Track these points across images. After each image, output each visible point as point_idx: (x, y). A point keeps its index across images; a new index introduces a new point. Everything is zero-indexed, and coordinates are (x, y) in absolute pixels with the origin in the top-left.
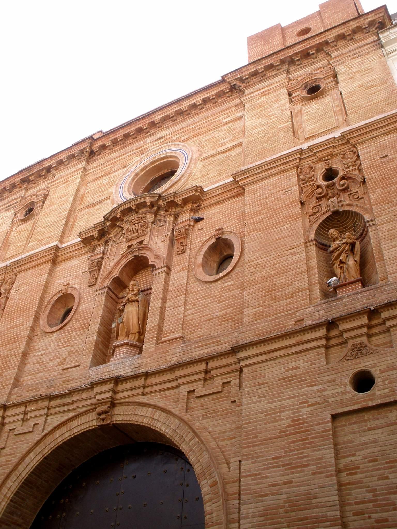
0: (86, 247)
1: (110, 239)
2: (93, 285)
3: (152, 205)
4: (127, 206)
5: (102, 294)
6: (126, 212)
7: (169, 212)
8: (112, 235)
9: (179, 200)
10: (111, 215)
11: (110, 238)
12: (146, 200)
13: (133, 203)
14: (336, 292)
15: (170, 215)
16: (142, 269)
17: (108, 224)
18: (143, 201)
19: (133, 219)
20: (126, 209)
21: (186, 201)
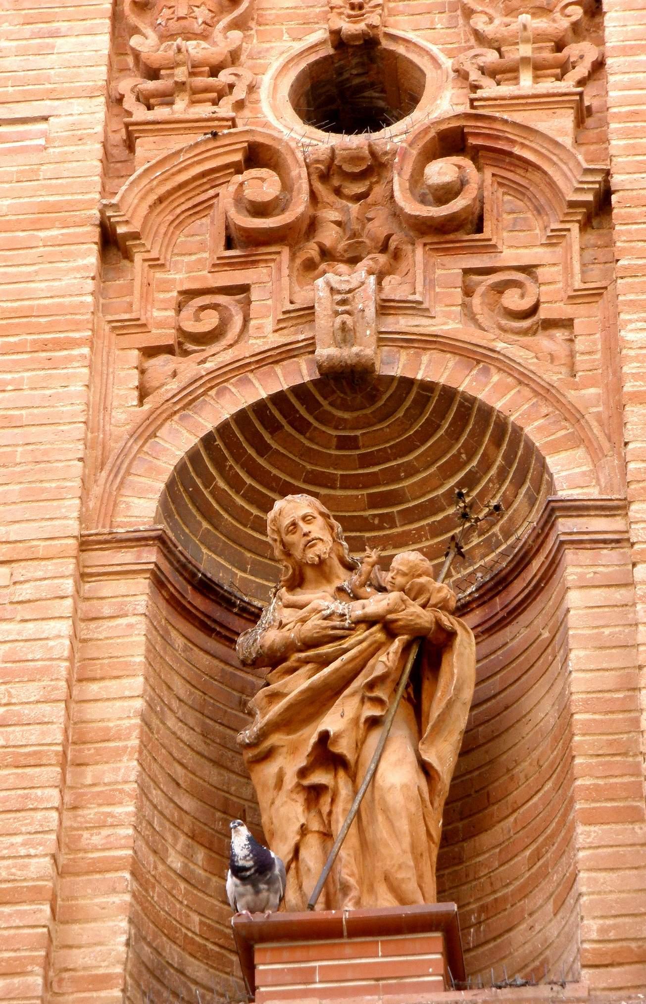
14: (249, 968)
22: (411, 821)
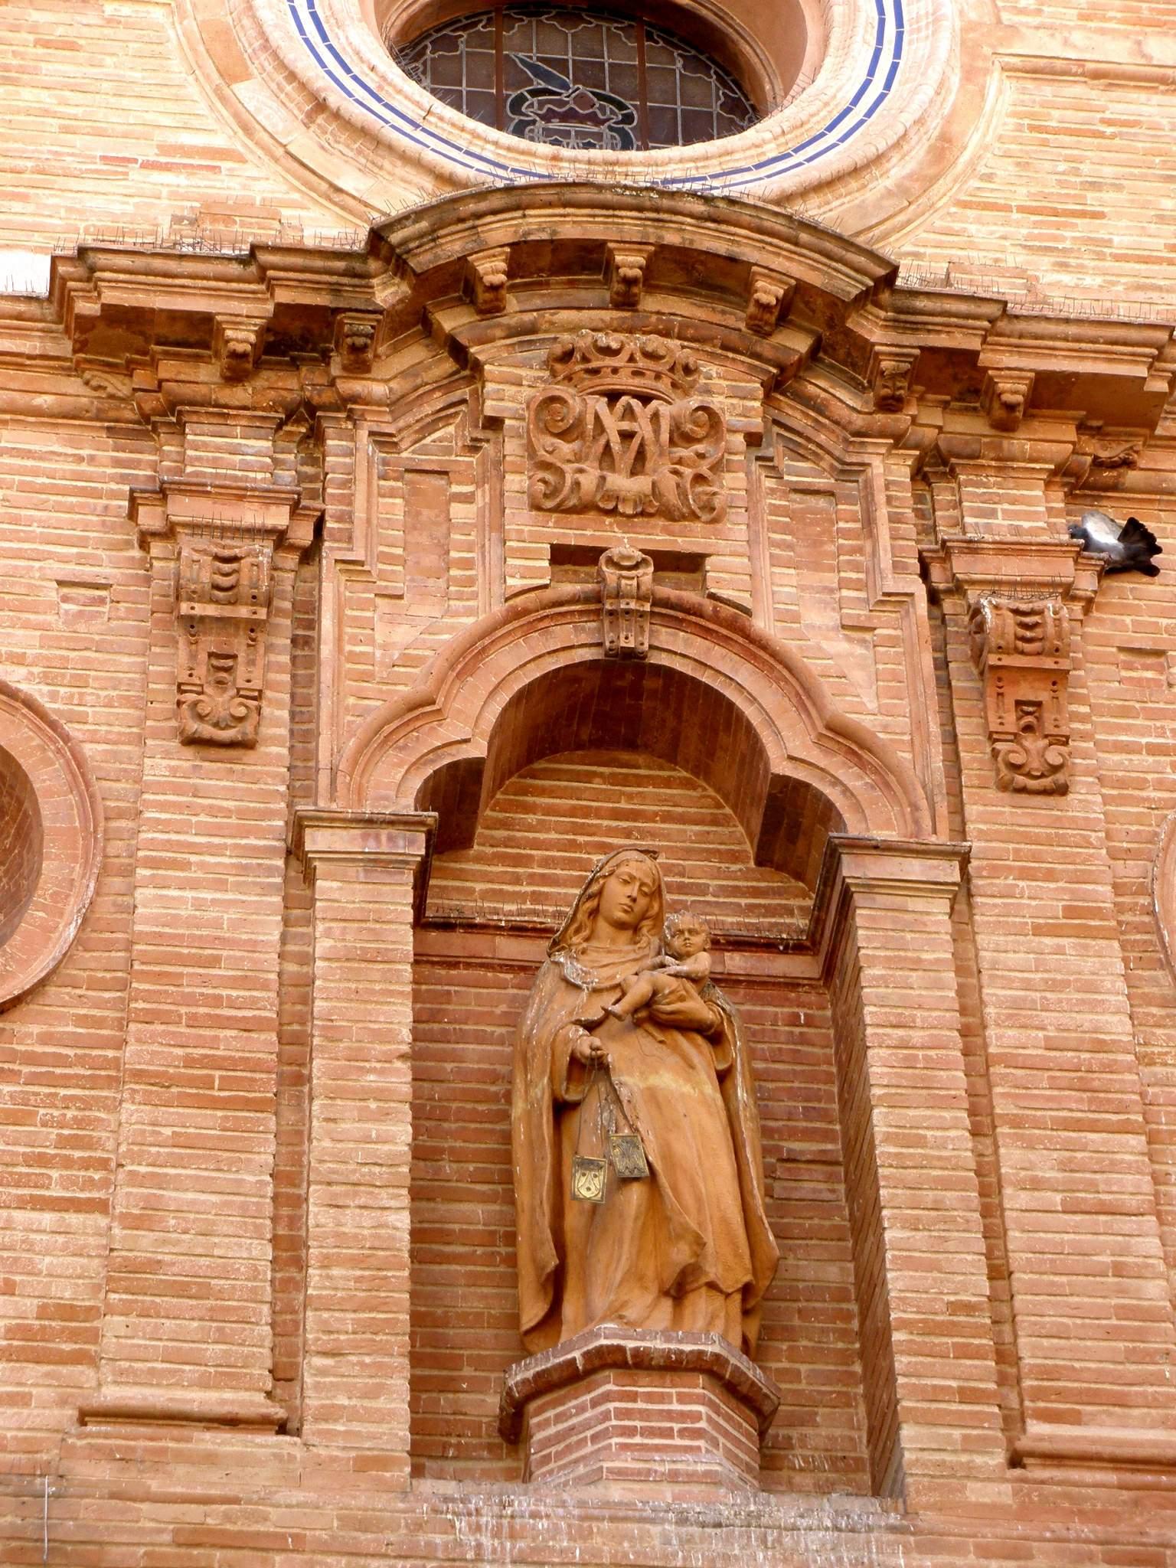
0: (76, 370)
1: (348, 406)
2: (232, 745)
3: (796, 304)
4: (574, 226)
5: (376, 863)
6: (546, 260)
7: (901, 420)
8: (379, 390)
9: (1012, 369)
10: (432, 235)
11: (355, 399)
12: (749, 253)
13: (630, 226)
15: (899, 440)
16: (580, 746)
17: (387, 293)
18: (721, 247)
19: (608, 351)
20: (557, 246)
21: (1050, 394)
22: (346, 517)
